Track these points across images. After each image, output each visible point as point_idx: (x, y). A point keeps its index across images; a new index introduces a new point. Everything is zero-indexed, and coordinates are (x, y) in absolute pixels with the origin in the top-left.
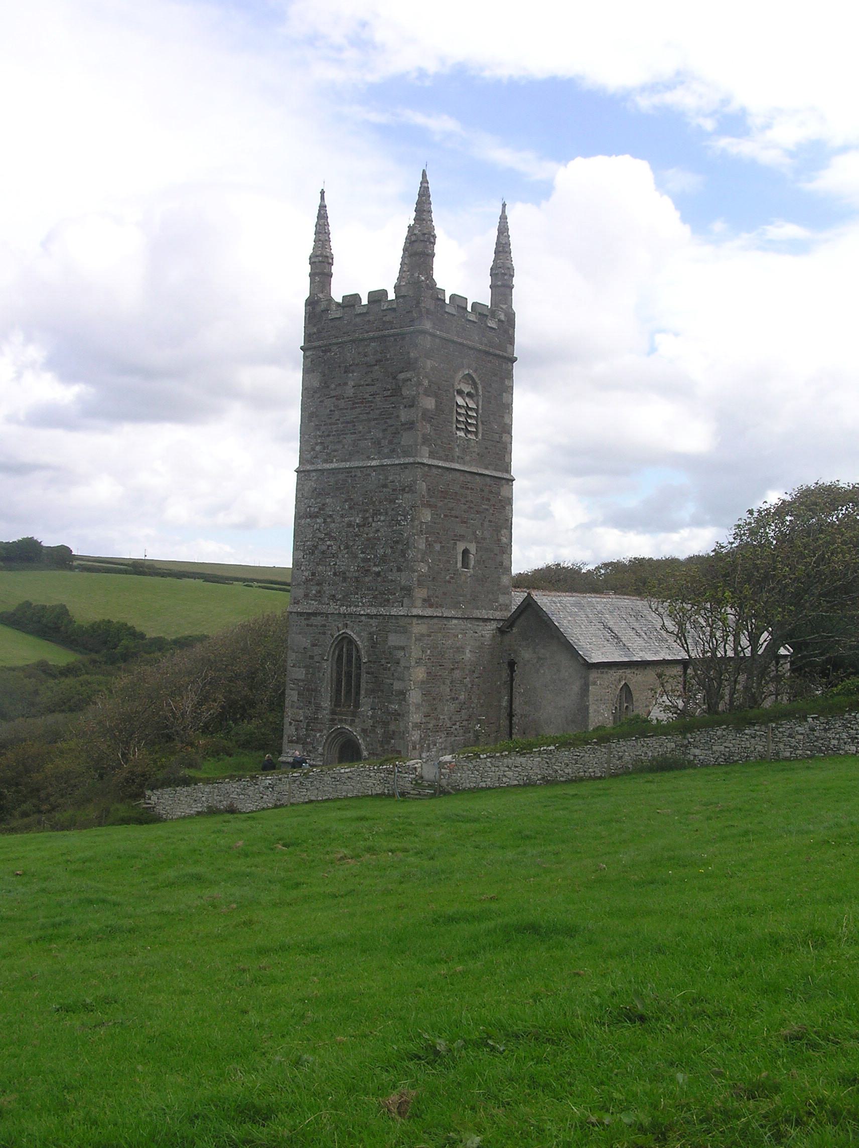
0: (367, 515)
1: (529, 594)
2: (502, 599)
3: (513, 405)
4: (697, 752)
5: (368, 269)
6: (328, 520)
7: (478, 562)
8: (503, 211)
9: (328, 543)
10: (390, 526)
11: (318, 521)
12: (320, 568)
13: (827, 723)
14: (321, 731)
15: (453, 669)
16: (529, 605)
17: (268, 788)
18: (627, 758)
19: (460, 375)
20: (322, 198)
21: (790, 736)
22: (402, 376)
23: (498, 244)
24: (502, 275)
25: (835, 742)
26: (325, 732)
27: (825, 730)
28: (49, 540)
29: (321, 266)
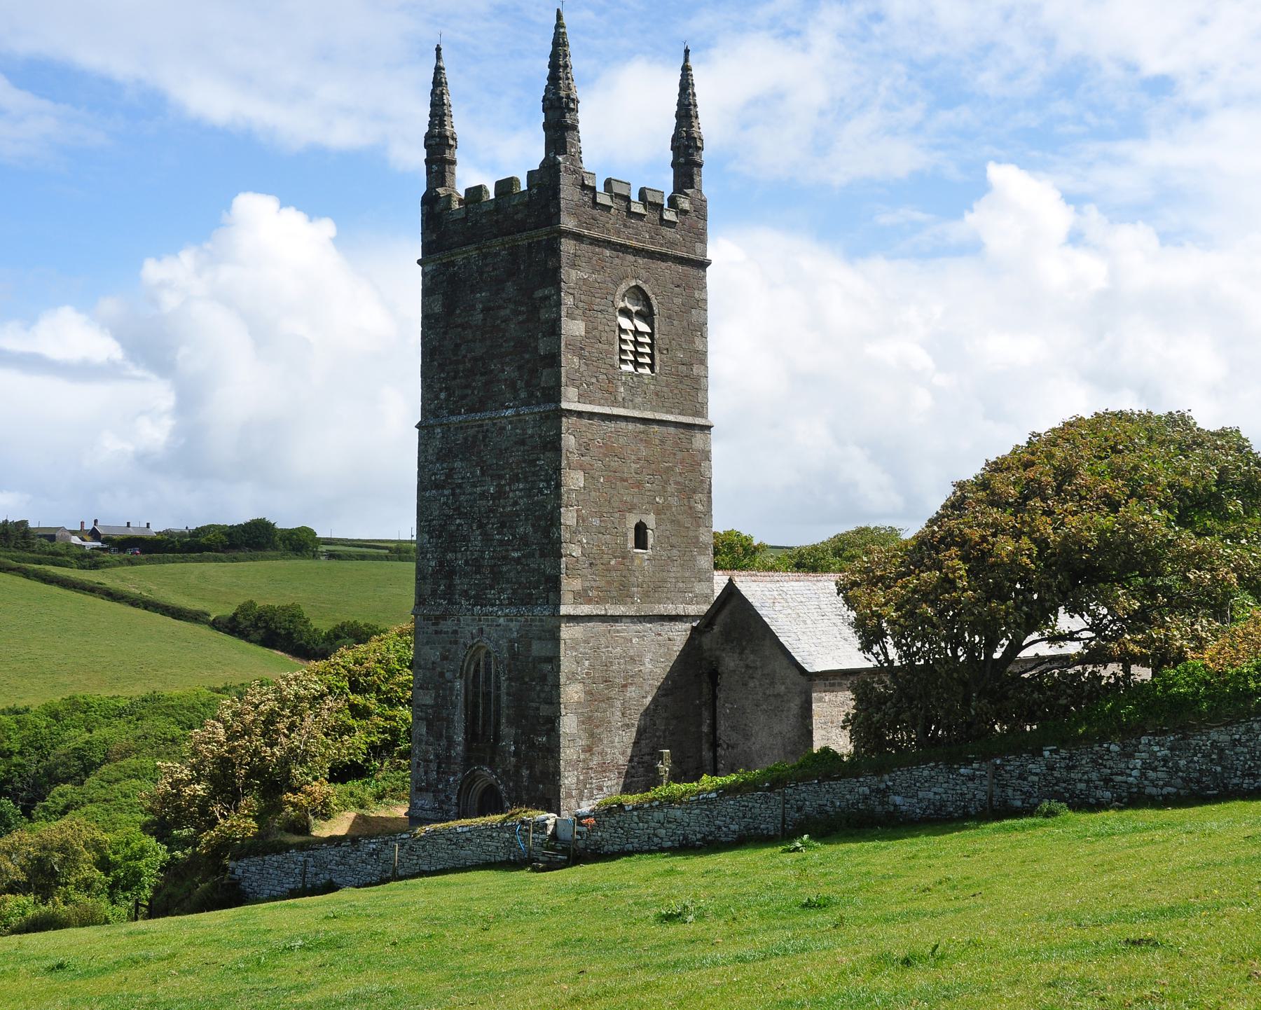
0: (503, 482)
1: (730, 580)
2: (700, 588)
3: (420, 315)
4: (898, 800)
5: (500, 151)
6: (458, 491)
7: (658, 539)
8: (686, 60)
9: (458, 521)
10: (529, 496)
11: (446, 492)
12: (450, 556)
13: (1070, 759)
14: (455, 774)
15: (625, 686)
16: (731, 591)
17: (372, 855)
18: (808, 809)
19: (623, 288)
20: (438, 57)
21: (1022, 777)
22: (539, 294)
23: (680, 104)
24: (686, 149)
25: (1082, 786)
26: (460, 775)
27: (1069, 768)
28: (284, 521)
29: (439, 148)
